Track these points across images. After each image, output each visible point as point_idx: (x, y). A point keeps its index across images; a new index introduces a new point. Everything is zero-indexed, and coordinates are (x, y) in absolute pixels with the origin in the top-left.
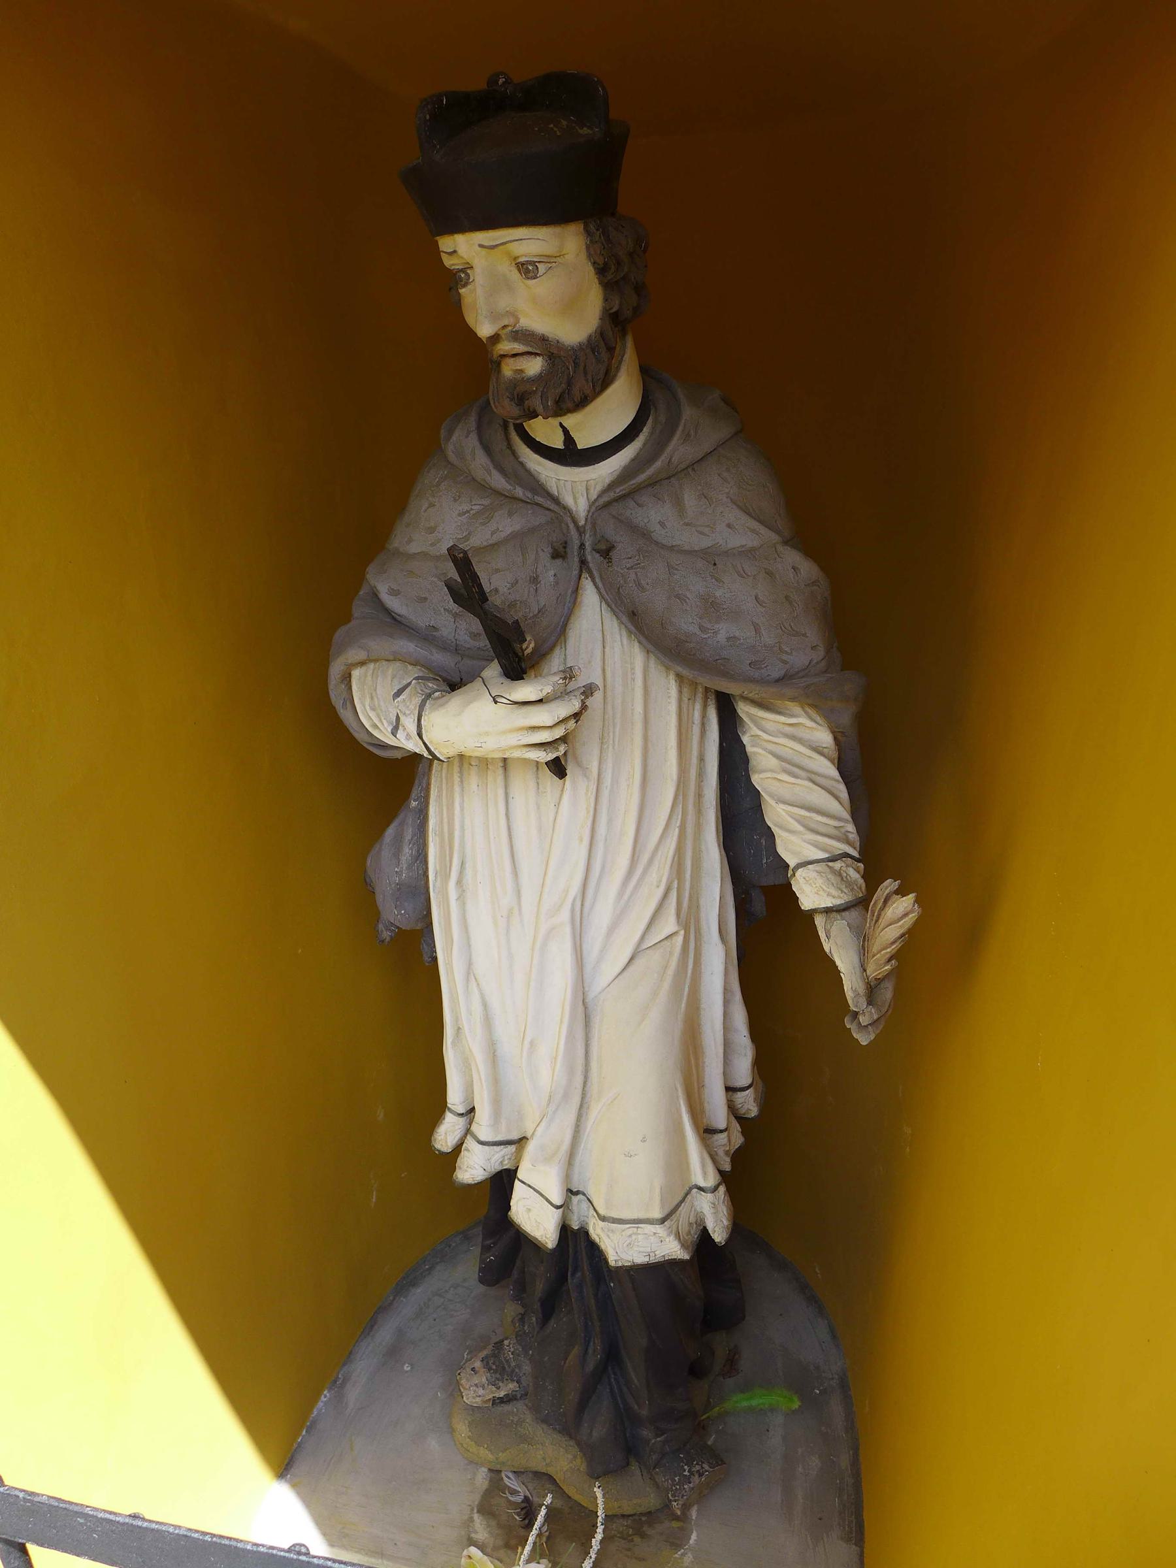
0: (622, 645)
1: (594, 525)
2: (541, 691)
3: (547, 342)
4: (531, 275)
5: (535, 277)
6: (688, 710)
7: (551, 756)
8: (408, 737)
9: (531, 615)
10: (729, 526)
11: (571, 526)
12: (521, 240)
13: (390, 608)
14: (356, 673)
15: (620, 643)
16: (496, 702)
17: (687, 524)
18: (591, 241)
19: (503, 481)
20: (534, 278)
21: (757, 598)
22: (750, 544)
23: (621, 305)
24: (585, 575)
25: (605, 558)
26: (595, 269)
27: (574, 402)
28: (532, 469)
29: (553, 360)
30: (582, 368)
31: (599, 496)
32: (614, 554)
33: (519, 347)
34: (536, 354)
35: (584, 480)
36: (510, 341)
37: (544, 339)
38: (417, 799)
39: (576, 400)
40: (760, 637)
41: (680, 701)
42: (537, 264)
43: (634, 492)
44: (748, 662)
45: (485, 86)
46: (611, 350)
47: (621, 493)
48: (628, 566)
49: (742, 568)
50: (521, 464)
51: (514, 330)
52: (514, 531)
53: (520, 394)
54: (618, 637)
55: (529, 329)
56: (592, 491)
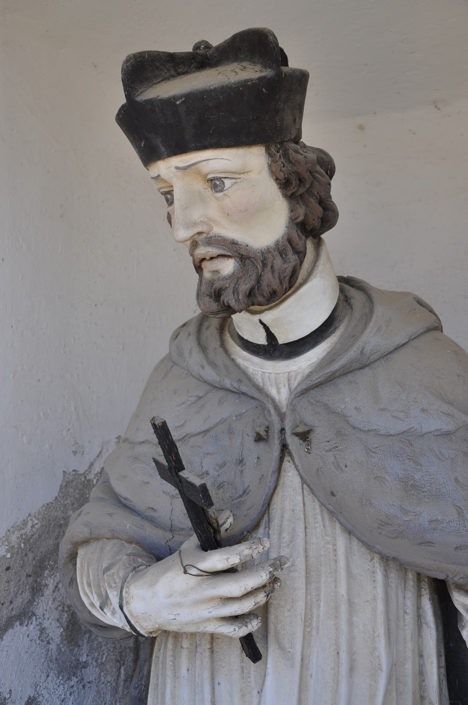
0: (324, 526)
1: (294, 410)
2: (227, 559)
3: (237, 246)
4: (219, 188)
5: (222, 190)
6: (397, 597)
7: (244, 631)
8: (114, 613)
9: (237, 495)
10: (423, 410)
11: (272, 411)
12: (208, 160)
13: (118, 492)
14: (81, 552)
15: (321, 523)
16: (185, 572)
17: (383, 410)
18: (273, 161)
19: (214, 374)
20: (221, 192)
21: (457, 480)
22: (445, 428)
23: (306, 215)
24: (287, 458)
25: (304, 441)
26: (278, 184)
27: (264, 296)
28: (241, 364)
29: (243, 261)
30: (269, 267)
31: (299, 385)
32: (312, 436)
33: (213, 251)
34: (229, 257)
35: (285, 371)
36: (205, 246)
37: (234, 243)
38: (138, 687)
39: (265, 295)
40: (464, 521)
41: (386, 585)
42: (223, 180)
43: (331, 380)
44: (455, 546)
45: (192, 51)
46: (301, 254)
47: (317, 381)
48: (327, 448)
49: (440, 452)
50: (233, 360)
51: (208, 236)
52: (223, 418)
53: (217, 292)
54: (319, 517)
55: (221, 235)
56: (292, 381)
